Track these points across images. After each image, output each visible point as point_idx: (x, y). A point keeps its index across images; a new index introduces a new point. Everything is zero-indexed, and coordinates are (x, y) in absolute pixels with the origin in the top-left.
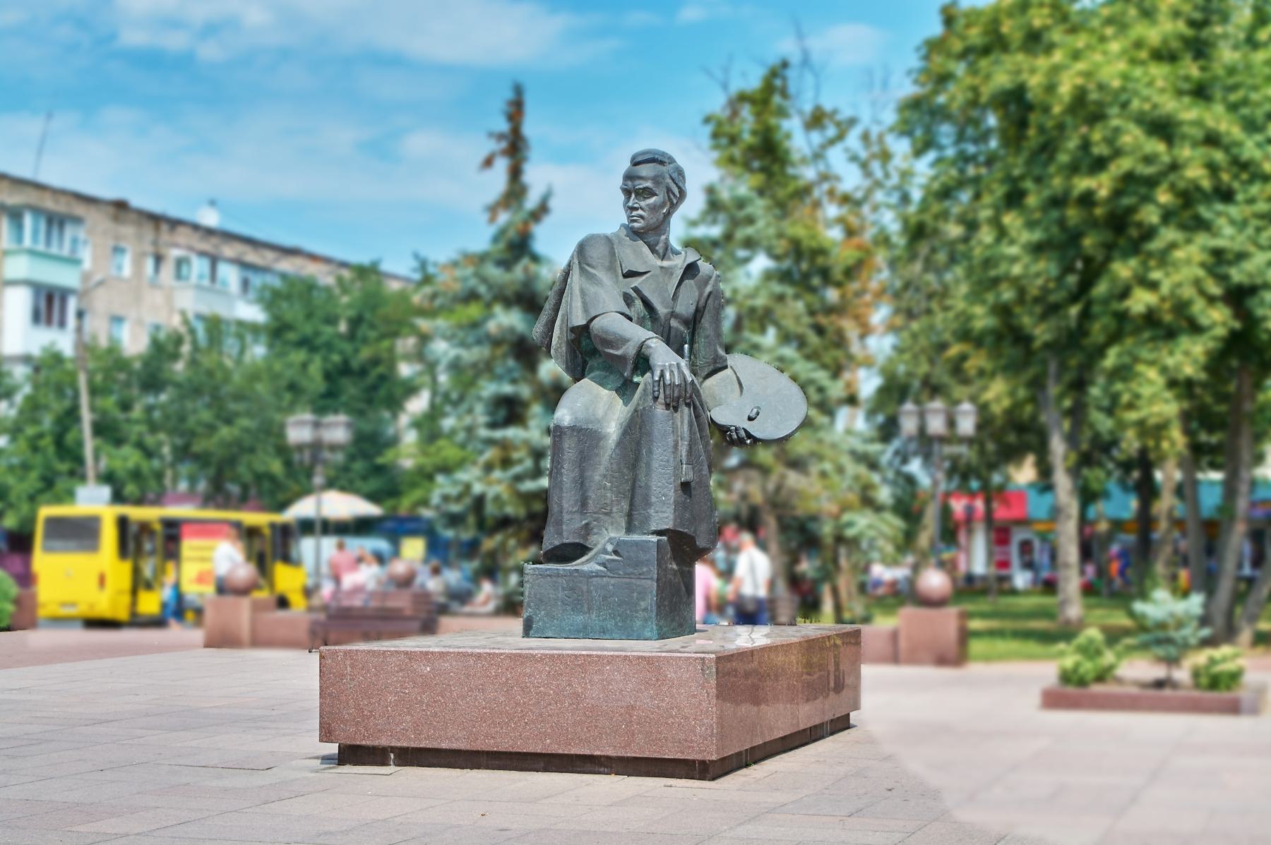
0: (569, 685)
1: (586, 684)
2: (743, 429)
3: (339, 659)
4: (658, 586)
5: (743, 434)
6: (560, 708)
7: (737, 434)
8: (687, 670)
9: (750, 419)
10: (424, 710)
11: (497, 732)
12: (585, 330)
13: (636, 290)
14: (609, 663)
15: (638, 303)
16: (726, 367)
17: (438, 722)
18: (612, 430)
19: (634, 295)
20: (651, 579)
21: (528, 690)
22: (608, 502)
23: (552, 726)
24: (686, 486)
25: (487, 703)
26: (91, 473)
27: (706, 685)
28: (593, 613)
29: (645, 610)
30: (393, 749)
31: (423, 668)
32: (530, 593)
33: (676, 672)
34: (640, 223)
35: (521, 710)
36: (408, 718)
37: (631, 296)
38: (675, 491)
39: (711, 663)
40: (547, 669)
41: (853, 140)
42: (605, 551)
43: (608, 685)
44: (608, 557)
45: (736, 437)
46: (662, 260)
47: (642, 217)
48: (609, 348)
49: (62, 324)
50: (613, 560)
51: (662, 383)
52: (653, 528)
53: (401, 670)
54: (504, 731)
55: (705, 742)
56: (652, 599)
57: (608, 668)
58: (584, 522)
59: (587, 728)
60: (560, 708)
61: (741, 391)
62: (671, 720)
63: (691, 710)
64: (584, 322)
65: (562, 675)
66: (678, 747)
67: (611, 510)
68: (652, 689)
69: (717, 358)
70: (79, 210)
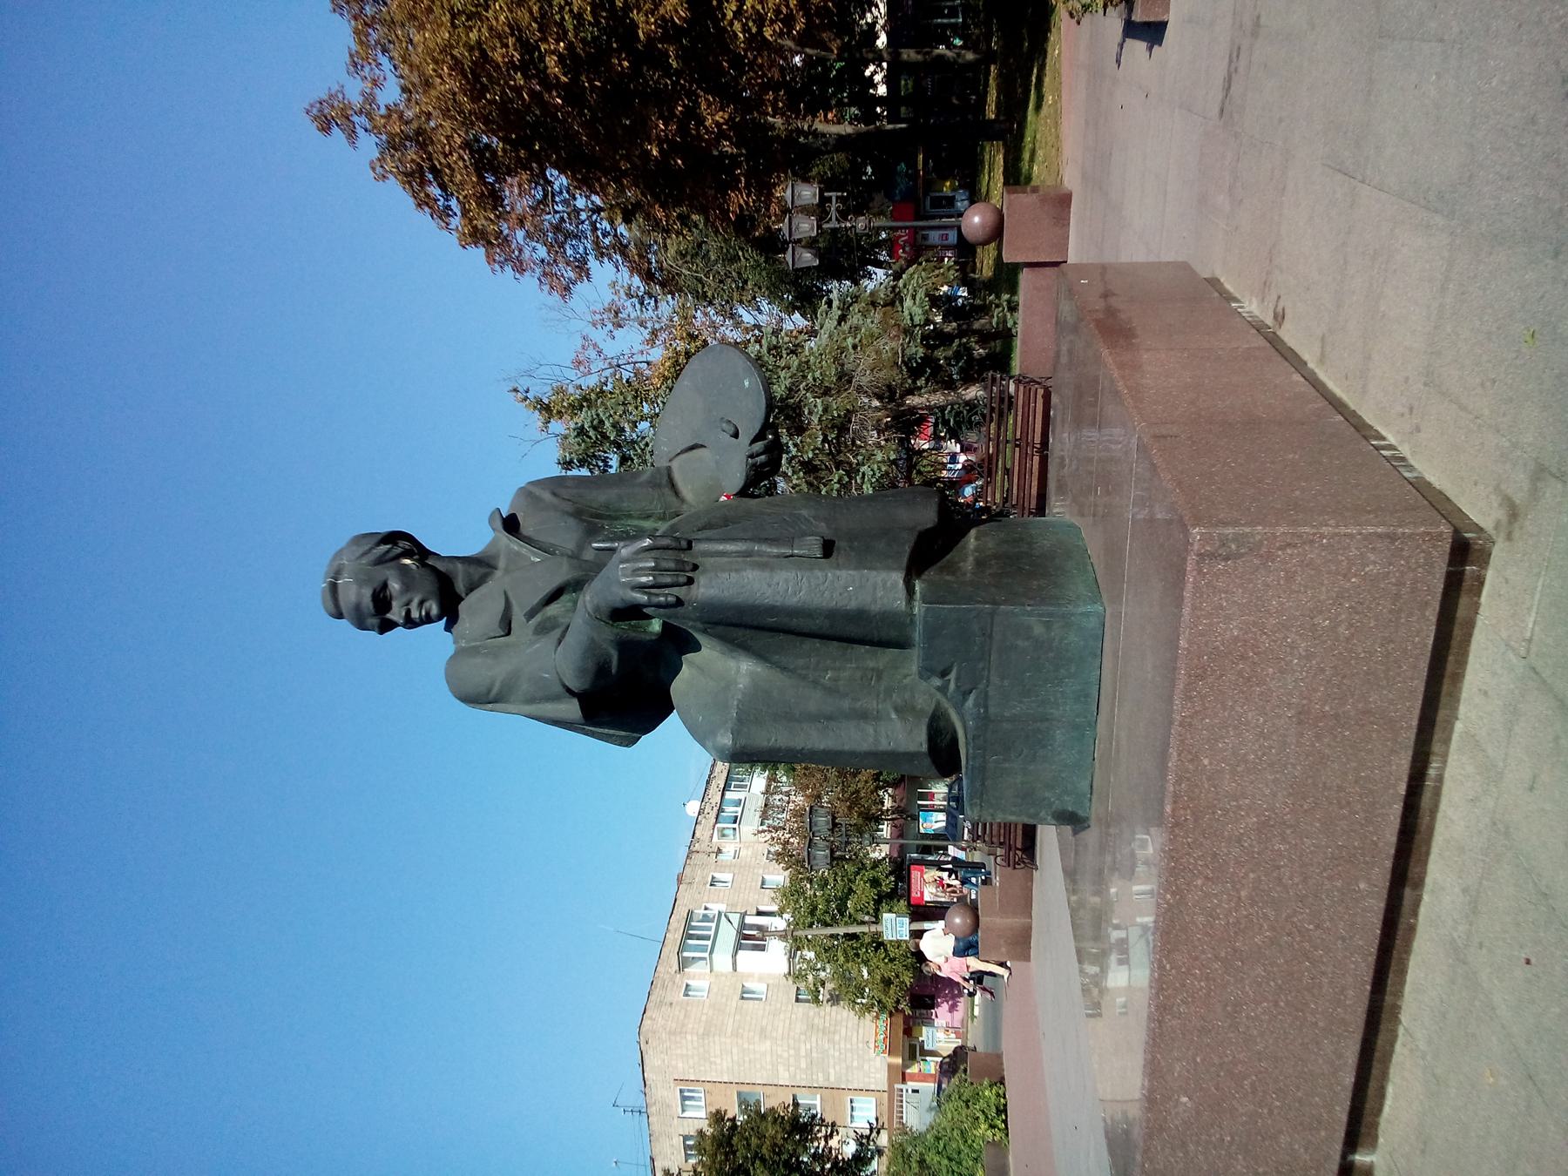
0: (1239, 841)
1: (1239, 807)
2: (751, 444)
4: (1005, 602)
5: (759, 446)
6: (1291, 860)
7: (758, 455)
8: (1226, 592)
9: (736, 435)
10: (1271, 1112)
11: (1331, 983)
12: (585, 698)
13: (531, 615)
14: (1195, 759)
15: (553, 609)
16: (669, 469)
17: (1298, 1089)
18: (743, 670)
19: (538, 618)
20: (992, 614)
21: (1243, 921)
22: (858, 674)
23: (1330, 878)
24: (828, 549)
25: (1266, 1000)
26: (873, 928)
28: (1052, 714)
29: (1048, 626)
30: (1344, 1156)
31: (1181, 1109)
32: (1013, 813)
33: (1229, 618)
34: (431, 606)
35: (1288, 935)
36: (1284, 1139)
37: (539, 624)
38: (838, 567)
39: (1212, 538)
40: (1199, 882)
41: (598, 335)
42: (943, 689)
43: (1246, 762)
44: (952, 686)
45: (763, 457)
46: (496, 569)
47: (421, 603)
48: (610, 667)
50: (958, 679)
51: (653, 591)
53: (1184, 1145)
56: (1030, 614)
57: (1206, 762)
58: (894, 716)
59: (1341, 808)
60: (1291, 860)
61: (702, 446)
62: (1341, 629)
63: (1322, 584)
64: (575, 702)
65: (1215, 855)
66: (1411, 614)
67: (873, 669)
68: (1262, 669)
69: (653, 484)
70: (681, 912)
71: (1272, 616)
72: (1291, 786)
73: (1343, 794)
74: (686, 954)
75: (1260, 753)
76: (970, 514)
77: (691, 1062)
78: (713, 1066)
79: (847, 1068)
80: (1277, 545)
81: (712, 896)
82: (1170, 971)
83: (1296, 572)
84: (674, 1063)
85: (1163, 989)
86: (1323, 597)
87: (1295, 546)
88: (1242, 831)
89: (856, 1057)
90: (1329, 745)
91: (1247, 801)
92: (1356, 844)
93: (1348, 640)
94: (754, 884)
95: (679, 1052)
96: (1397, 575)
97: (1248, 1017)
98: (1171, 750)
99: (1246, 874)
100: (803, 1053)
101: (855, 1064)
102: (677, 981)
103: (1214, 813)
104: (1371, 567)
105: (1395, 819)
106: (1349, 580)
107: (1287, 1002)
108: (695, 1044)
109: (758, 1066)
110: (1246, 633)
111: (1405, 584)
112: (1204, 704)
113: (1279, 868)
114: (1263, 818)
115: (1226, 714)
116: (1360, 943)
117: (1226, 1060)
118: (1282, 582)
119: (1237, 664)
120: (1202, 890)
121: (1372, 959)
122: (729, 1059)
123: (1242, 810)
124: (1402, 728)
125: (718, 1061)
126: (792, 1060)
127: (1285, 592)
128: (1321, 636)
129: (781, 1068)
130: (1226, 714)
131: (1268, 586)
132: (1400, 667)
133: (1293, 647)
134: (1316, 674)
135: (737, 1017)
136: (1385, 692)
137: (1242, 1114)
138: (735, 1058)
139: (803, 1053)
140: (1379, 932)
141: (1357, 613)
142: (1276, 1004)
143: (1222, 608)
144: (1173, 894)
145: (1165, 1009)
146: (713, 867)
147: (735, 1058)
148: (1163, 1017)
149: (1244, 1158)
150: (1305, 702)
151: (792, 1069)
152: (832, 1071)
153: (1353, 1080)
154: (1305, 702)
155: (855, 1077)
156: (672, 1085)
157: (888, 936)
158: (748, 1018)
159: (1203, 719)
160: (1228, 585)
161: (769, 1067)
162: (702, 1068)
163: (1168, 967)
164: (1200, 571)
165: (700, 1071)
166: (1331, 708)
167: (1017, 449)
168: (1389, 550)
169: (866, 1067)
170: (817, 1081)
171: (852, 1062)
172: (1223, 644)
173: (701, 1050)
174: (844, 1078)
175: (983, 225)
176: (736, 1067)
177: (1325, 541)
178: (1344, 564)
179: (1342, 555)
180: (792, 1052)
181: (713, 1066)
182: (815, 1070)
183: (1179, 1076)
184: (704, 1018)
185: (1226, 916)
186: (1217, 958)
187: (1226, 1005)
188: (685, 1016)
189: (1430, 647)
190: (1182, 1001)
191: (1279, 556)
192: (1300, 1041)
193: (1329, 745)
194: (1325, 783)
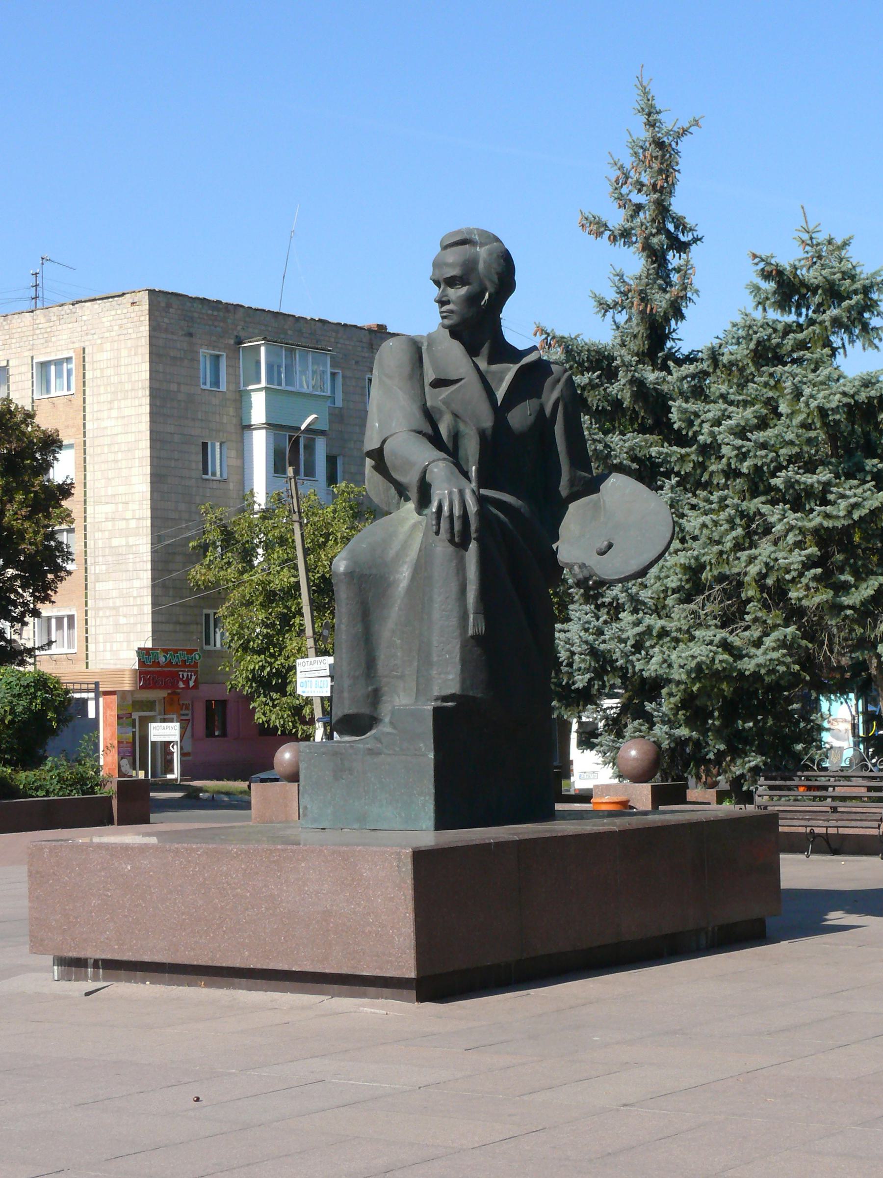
0: (265, 886)
1: (282, 884)
3: (45, 856)
10: (126, 916)
11: (196, 942)
27: (403, 884)
31: (124, 866)
36: (111, 925)
49: (310, 472)
52: (436, 694)
54: (203, 941)
55: (404, 956)
57: (303, 865)
58: (370, 689)
64: (379, 446)
77: (109, 372)
79: (115, 608)
84: (108, 346)
89: (132, 620)
93: (363, 932)
95: (124, 353)
97: (175, 899)
99: (249, 891)
100: (132, 540)
101: (122, 620)
107: (185, 919)
108: (135, 377)
109: (110, 474)
113: (253, 908)
116: (218, 956)
117: (152, 889)
125: (114, 413)
126: (122, 524)
129: (110, 508)
133: (359, 905)
135: (177, 438)
138: (120, 439)
139: (132, 540)
142: (183, 914)
143: (376, 866)
144: (236, 853)
147: (120, 439)
151: (109, 525)
152: (109, 585)
155: (104, 621)
156: (77, 345)
161: (110, 491)
162: (102, 390)
163: (199, 853)
164: (392, 853)
165: (99, 386)
169: (120, 637)
170: (95, 563)
171: (125, 616)
172: (360, 868)
173: (128, 387)
174: (101, 604)
176: (107, 440)
180: (133, 524)
184: (174, 387)
186: (205, 879)
187: (180, 886)
189: (361, 974)
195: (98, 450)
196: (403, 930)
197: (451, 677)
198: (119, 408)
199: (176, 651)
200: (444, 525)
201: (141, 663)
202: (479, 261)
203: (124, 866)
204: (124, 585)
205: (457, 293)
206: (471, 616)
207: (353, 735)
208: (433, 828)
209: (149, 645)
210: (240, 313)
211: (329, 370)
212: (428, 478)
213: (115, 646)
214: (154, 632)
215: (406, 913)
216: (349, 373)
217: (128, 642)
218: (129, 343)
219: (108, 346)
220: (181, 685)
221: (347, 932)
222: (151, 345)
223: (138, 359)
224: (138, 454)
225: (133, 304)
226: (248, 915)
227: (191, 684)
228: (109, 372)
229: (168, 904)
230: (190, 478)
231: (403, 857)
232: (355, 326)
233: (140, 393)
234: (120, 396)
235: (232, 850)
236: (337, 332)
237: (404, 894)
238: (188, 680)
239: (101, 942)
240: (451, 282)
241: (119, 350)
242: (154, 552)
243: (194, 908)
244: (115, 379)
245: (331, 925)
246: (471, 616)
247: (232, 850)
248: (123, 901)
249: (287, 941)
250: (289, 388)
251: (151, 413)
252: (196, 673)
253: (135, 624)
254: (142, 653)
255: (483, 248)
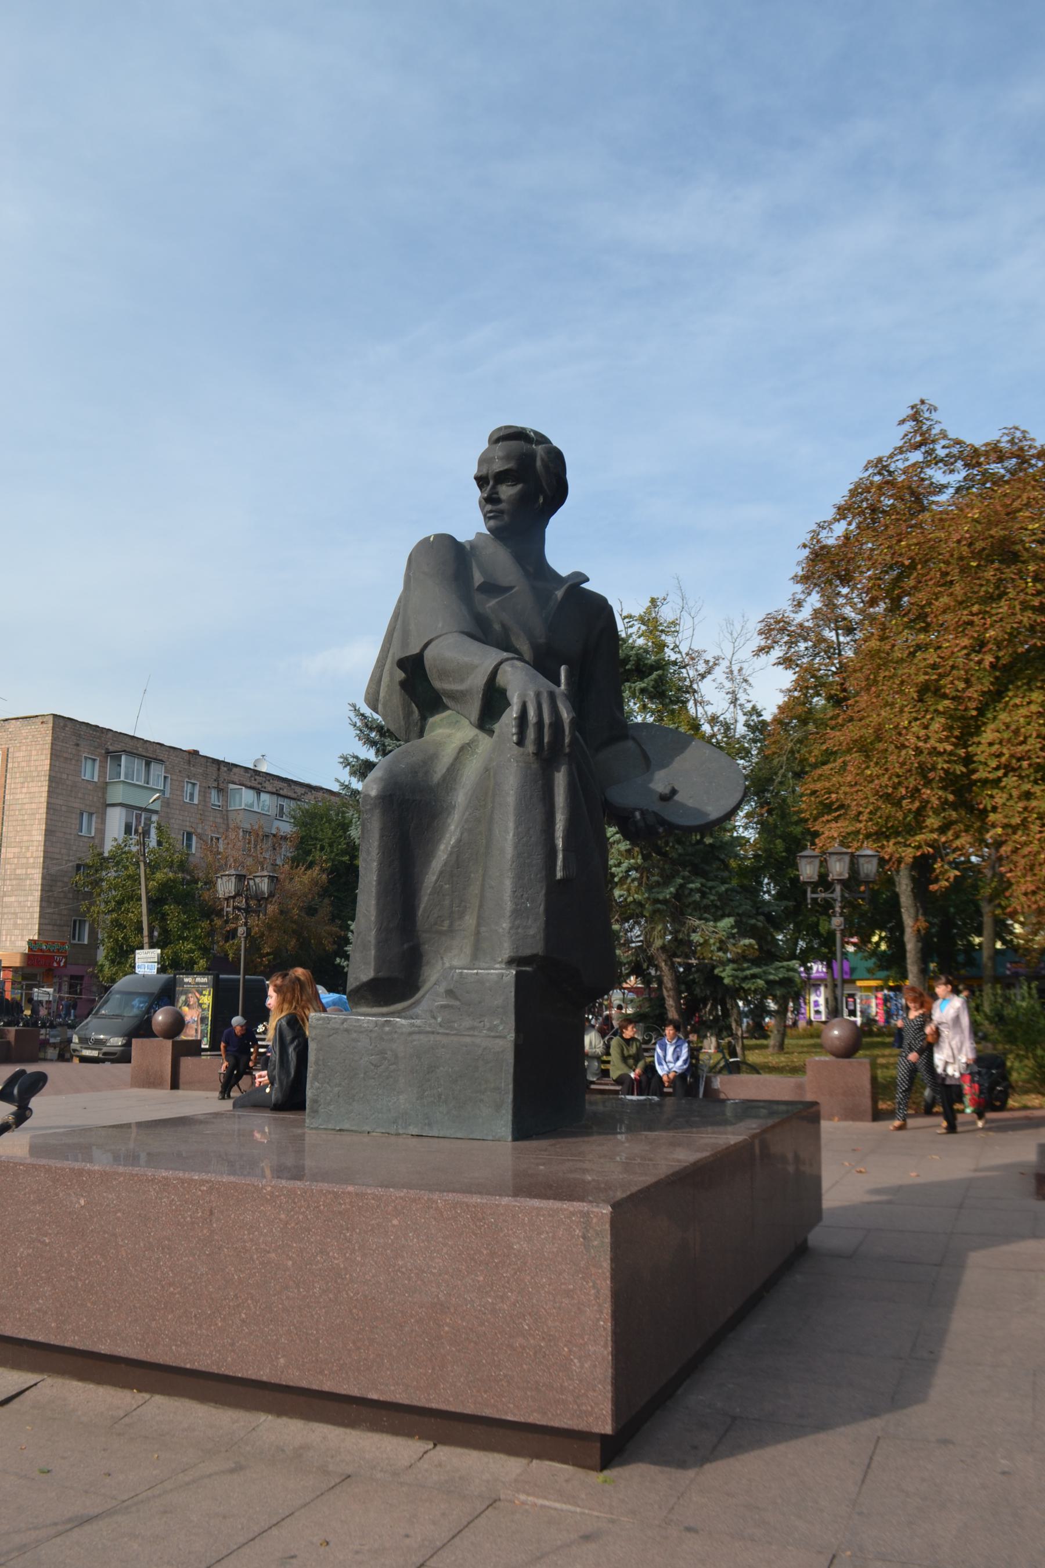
1: (353, 1251)
10: (72, 1278)
31: (74, 1199)
35: (236, 1296)
40: (283, 1216)
58: (406, 946)
65: (309, 1230)
71: (532, 1278)
72: (374, 1298)
73: (366, 1343)
74: (123, 758)
75: (404, 1270)
76: (955, 926)
78: (19, 786)
79: (15, 914)
80: (598, 1282)
81: (177, 783)
82: (200, 1190)
83: (573, 1298)
84: (24, 748)
85: (183, 1183)
86: (550, 1323)
87: (597, 1297)
88: (331, 1254)
89: (26, 922)
90: (412, 1331)
91: (359, 1259)
92: (321, 1355)
94: (188, 824)
95: (34, 753)
96: (571, 1387)
98: (405, 1190)
100: (29, 871)
101: (19, 921)
102: (98, 750)
103: (347, 1229)
104: (578, 1364)
105: (345, 1389)
106: (565, 1345)
107: (172, 1293)
108: (40, 768)
110: (516, 1256)
111: (562, 1394)
112: (449, 1219)
114: (343, 1273)
115: (440, 1239)
117: (119, 1239)
118: (563, 1287)
119: (486, 1249)
120: (275, 1218)
121: (214, 1369)
122: (25, 801)
123: (351, 1254)
124: (429, 1394)
125: (24, 790)
127: (554, 1290)
128: (514, 1322)
129: (16, 850)
130: (440, 1239)
131: (560, 1274)
132: (485, 1392)
134: (477, 1318)
135: (64, 808)
136: (462, 1380)
137: (69, 1253)
138: (26, 806)
139: (29, 871)
140: (240, 1375)
141: (535, 1353)
142: (170, 1284)
143: (539, 1234)
144: (271, 1193)
145: (164, 1185)
146: (204, 785)
148: (157, 1184)
149: (29, 1255)
150: (452, 1310)
152: (13, 899)
153: (103, 1352)
154: (452, 1310)
157: (140, 954)
158: (63, 819)
159: (435, 1219)
160: (560, 1239)
164: (573, 1214)
165: (16, 773)
166: (447, 1333)
167: (851, 1000)
168: (594, 1379)
169: (17, 932)
171: (21, 918)
173: (35, 774)
175: (838, 1038)
176: (18, 807)
177: (602, 1323)
178: (581, 1341)
179: (589, 1339)
180: (31, 860)
181: (19, 786)
182: (14, 882)
183: (104, 1198)
184: (64, 776)
185: (252, 1240)
187: (169, 1240)
188: (66, 758)
189: (504, 1417)
190: (173, 1200)
191: (587, 1283)
192: (138, 1305)
193: (412, 1331)
194: (377, 1327)
195: (12, 813)
196: (592, 1349)
197: (532, 932)
198: (28, 787)
199: (53, 943)
200: (531, 734)
201: (30, 949)
202: (536, 457)
203: (74, 1199)
204: (22, 899)
205: (507, 491)
206: (560, 856)
207: (381, 1006)
208: (510, 1138)
209: (36, 938)
210: (110, 735)
211: (163, 775)
212: (500, 680)
213: (13, 938)
214: (39, 930)
215: (598, 1320)
216: (175, 777)
217: (22, 936)
218: (38, 747)
219: (24, 748)
220: (55, 965)
221: (476, 1343)
222: (52, 749)
223: (43, 757)
224: (37, 816)
225: (42, 723)
226: (288, 1298)
227: (62, 964)
228: (24, 764)
229: (144, 1266)
230: (71, 834)
231: (594, 1220)
232: (181, 750)
233: (42, 778)
234: (29, 780)
235: (264, 1187)
236: (169, 752)
237: (594, 1287)
238: (60, 961)
239: (29, 1314)
240: (501, 477)
241: (31, 750)
242: (43, 878)
243: (190, 1277)
244: (27, 769)
245: (447, 1329)
246: (560, 856)
247: (264, 1187)
248: (69, 1253)
249: (359, 1348)
250: (138, 783)
251: (49, 791)
252: (66, 957)
253: (28, 924)
254: (31, 942)
255: (540, 447)
